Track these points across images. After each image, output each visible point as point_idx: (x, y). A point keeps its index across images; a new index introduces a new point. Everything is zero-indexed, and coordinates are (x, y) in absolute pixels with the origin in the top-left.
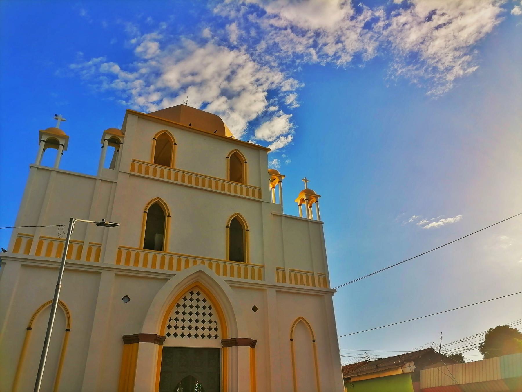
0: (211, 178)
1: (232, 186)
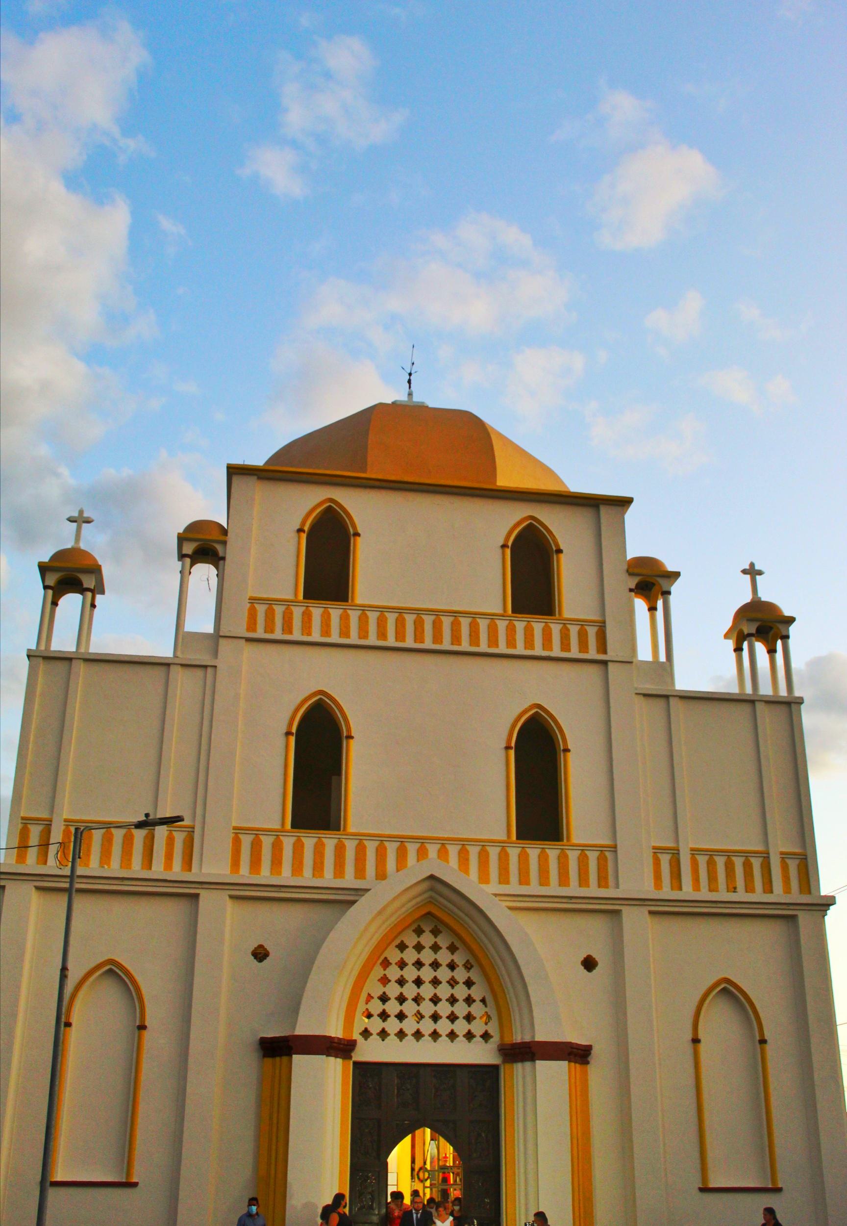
0: (455, 614)
1: (520, 626)
